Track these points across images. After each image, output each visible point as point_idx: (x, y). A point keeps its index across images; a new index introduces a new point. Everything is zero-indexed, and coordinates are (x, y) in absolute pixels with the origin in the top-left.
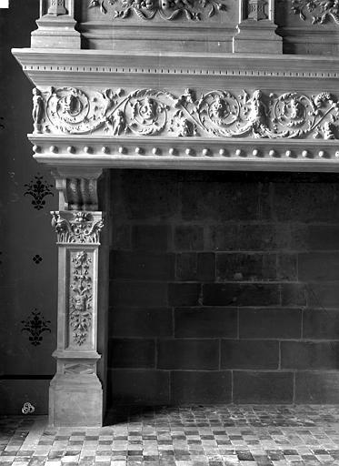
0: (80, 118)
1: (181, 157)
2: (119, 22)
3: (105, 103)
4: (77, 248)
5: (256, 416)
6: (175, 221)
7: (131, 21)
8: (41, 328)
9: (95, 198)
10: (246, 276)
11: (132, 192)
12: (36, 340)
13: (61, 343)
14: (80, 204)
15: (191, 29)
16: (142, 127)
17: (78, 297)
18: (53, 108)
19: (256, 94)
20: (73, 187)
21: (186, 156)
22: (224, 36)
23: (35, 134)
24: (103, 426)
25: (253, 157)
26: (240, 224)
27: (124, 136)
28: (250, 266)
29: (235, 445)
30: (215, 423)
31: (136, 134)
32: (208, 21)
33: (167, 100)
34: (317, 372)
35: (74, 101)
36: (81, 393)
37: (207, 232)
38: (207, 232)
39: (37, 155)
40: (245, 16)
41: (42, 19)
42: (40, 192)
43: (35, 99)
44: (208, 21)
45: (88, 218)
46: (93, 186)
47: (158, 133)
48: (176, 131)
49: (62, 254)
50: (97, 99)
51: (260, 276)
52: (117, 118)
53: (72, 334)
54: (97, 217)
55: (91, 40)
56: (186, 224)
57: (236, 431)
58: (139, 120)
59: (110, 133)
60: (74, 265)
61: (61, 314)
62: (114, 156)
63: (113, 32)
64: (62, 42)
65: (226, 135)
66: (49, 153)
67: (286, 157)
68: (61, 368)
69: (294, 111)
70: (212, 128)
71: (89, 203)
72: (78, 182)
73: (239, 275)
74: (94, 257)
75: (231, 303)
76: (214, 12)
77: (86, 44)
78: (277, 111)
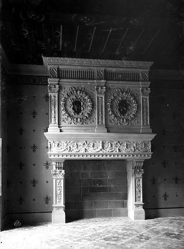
0: (60, 148)
1: (76, 157)
2: (69, 125)
3: (66, 144)
4: (58, 179)
5: (103, 220)
6: (82, 171)
7: (71, 125)
8: (48, 200)
9: (62, 166)
10: (100, 185)
11: (71, 166)
12: (47, 203)
13: (54, 203)
14: (59, 168)
15: (86, 127)
16: (74, 150)
17: (59, 191)
18: (53, 146)
19: (101, 142)
20: (57, 164)
21: (85, 157)
22: (93, 128)
23: (49, 152)
24: (147, 218)
25: (101, 157)
26: (98, 171)
27: (70, 152)
28: (100, 182)
29: (98, 225)
30: (93, 221)
31: (73, 152)
32: (89, 124)
33: (80, 144)
34: (118, 209)
35: (58, 144)
36: (59, 214)
37: (89, 174)
38: (89, 174)
39: (49, 157)
40: (98, 124)
41: (50, 125)
42: (47, 165)
43: (49, 144)
44: (89, 124)
45: (61, 172)
46: (62, 164)
47: (78, 152)
48: (83, 151)
49: (54, 180)
50: (64, 145)
51: (103, 184)
52: (69, 148)
53: (57, 200)
54: (63, 171)
55: (151, 130)
56: (84, 172)
57: (98, 223)
58: (74, 149)
59: (67, 152)
60: (57, 184)
61: (54, 196)
62: (68, 157)
63: (67, 128)
64: (55, 130)
65: (94, 152)
66: (52, 157)
67: (108, 157)
68: (54, 209)
69: (110, 146)
70: (91, 150)
71: (61, 168)
72: (59, 163)
73: (98, 185)
74: (62, 181)
75: (96, 192)
76: (91, 122)
77: (61, 131)
78: (106, 146)
